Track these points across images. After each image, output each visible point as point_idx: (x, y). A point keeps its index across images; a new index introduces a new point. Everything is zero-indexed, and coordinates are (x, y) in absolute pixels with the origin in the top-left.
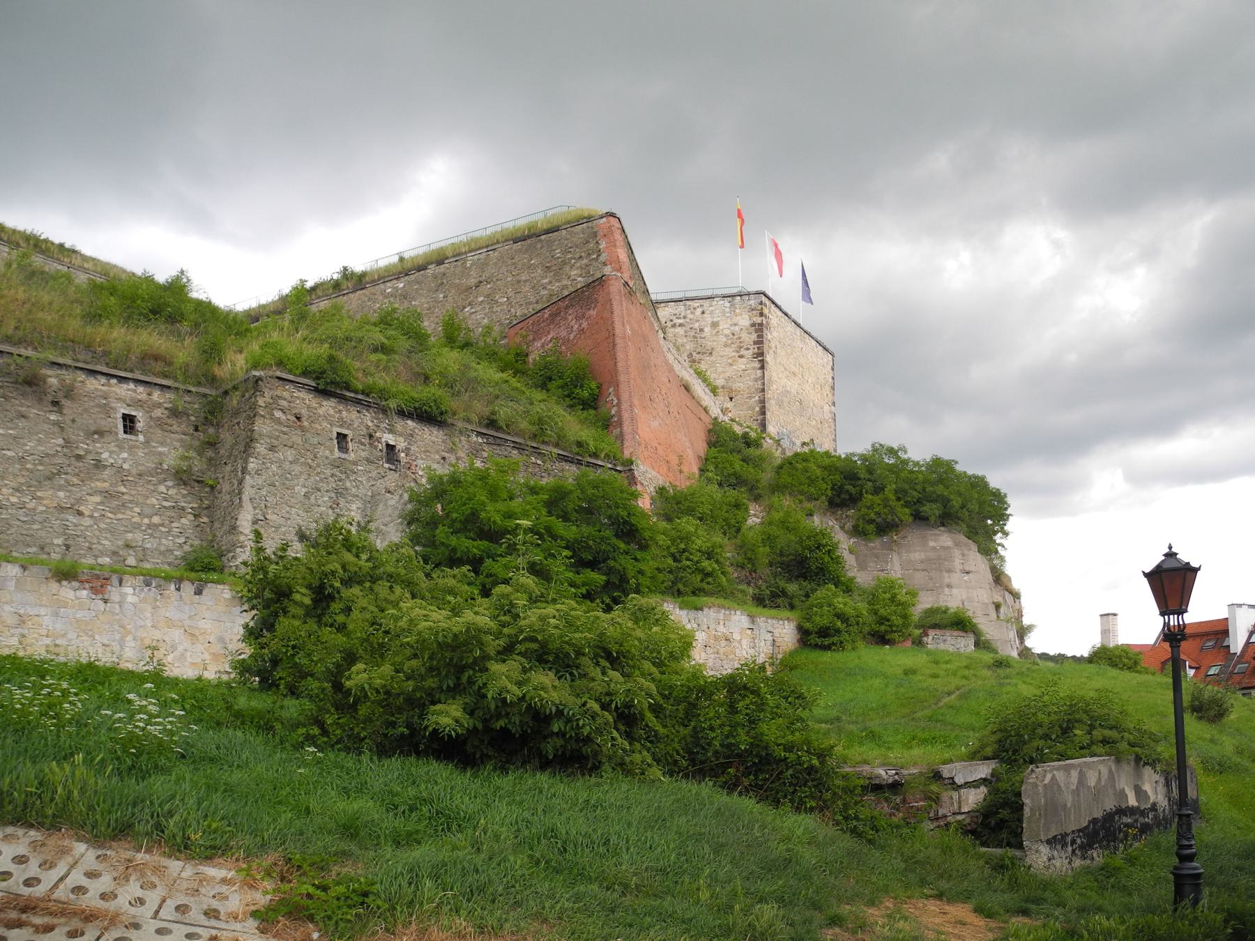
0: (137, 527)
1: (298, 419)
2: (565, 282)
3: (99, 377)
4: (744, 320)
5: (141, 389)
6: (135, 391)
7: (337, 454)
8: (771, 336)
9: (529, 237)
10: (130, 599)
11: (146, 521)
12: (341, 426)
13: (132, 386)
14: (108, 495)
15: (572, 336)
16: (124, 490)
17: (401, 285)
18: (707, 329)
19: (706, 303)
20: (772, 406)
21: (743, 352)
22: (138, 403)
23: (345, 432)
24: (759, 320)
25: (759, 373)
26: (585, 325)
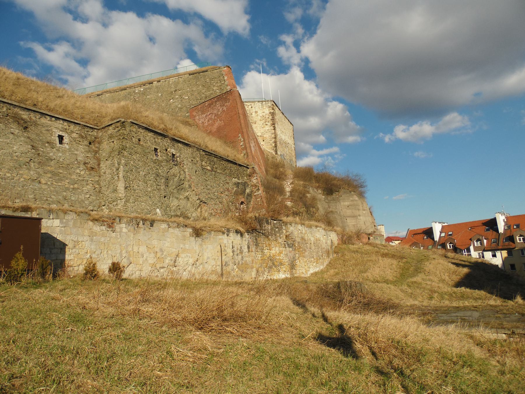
0: (68, 189)
1: (139, 141)
2: (211, 92)
3: (47, 117)
4: (267, 111)
5: (66, 124)
6: (63, 124)
7: (155, 158)
8: (277, 117)
9: (196, 73)
10: (124, 230)
11: (72, 186)
12: (155, 145)
13: (61, 122)
14: (54, 174)
15: (219, 113)
16: (61, 171)
17: (142, 89)
18: (254, 114)
19: (253, 104)
20: (278, 144)
21: (267, 123)
22: (65, 130)
23: (157, 147)
24: (272, 111)
25: (273, 131)
26: (225, 108)
